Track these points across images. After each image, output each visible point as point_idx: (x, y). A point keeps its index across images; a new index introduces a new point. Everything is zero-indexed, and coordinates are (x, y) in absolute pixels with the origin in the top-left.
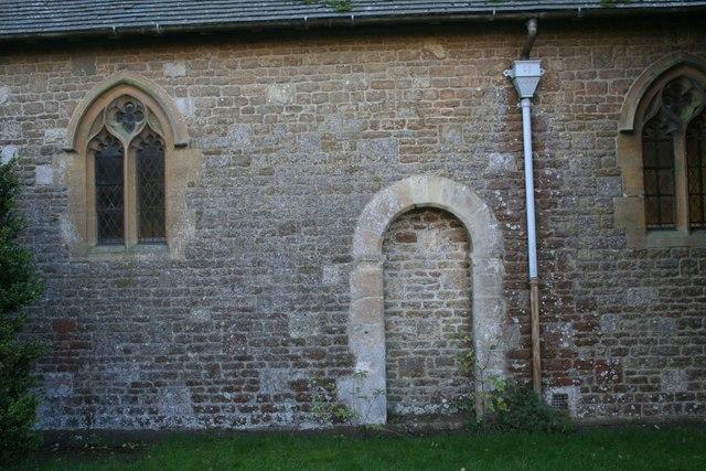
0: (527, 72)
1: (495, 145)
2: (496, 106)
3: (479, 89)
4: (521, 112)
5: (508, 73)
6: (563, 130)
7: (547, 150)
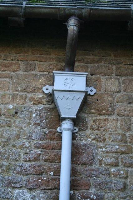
0: (70, 85)
1: (22, 179)
2: (30, 128)
3: (11, 107)
4: (61, 138)
5: (47, 89)
6: (116, 165)
7: (93, 190)
